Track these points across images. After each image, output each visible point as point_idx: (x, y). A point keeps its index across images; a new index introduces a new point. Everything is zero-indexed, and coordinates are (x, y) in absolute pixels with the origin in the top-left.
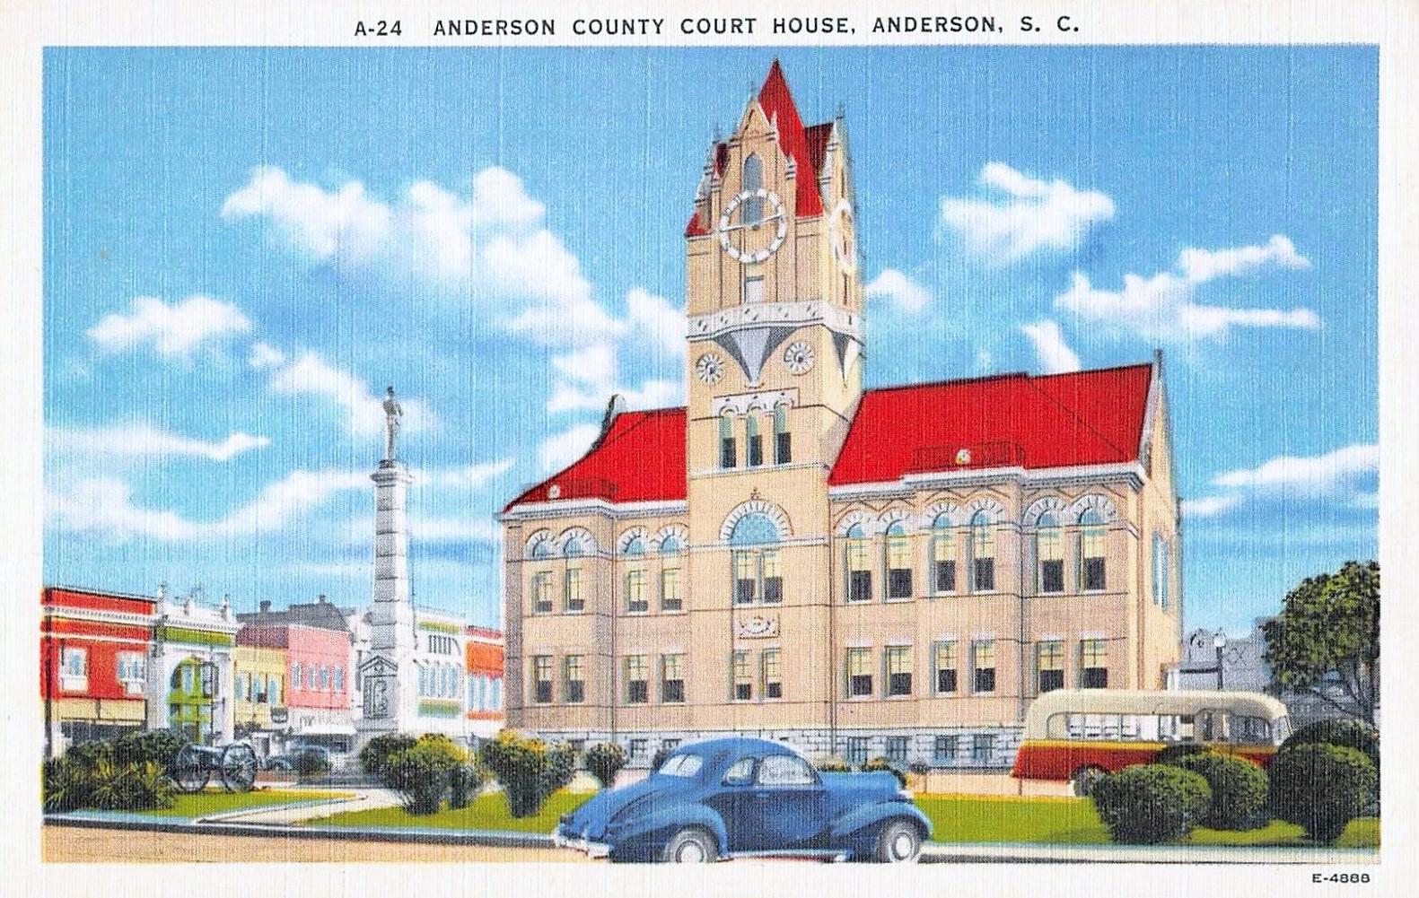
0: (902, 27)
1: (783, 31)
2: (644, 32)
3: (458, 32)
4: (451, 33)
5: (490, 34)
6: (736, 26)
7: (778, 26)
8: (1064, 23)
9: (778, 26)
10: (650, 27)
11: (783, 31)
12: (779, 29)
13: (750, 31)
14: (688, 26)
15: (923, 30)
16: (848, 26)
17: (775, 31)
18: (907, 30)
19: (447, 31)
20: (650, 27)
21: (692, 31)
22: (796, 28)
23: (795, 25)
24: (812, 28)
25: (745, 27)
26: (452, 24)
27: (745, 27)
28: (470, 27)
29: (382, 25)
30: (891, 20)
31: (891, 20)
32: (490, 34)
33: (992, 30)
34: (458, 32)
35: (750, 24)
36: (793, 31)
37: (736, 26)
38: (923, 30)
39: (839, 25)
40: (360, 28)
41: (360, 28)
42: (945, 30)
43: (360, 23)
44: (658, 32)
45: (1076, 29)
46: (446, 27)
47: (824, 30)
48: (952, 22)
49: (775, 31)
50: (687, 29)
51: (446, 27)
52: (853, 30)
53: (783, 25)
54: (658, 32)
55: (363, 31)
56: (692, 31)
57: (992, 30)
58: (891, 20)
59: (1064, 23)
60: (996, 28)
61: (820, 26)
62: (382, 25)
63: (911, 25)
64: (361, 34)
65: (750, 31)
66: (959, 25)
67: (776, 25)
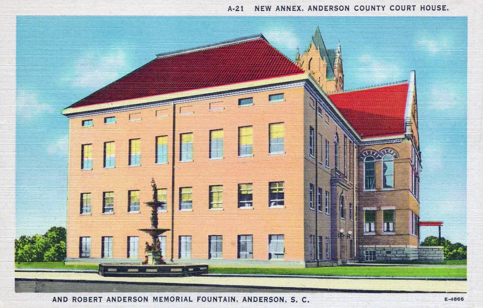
0: (63, 300)
1: (424, 10)
2: (378, 10)
3: (251, 301)
4: (248, 301)
5: (264, 11)
6: (409, 8)
7: (422, 8)
8: (304, 300)
9: (422, 8)
10: (381, 8)
11: (424, 10)
12: (423, 9)
13: (414, 10)
14: (392, 8)
15: (260, 301)
16: (446, 8)
17: (421, 10)
18: (320, 10)
19: (280, 10)
20: (381, 8)
21: (358, 10)
22: (321, 9)
23: (428, 8)
24: (210, 300)
25: (412, 8)
26: (314, 7)
27: (412, 8)
28: (321, 8)
29: (237, 7)
30: (282, 7)
31: (282, 7)
32: (264, 11)
33: (283, 301)
34: (251, 301)
35: (378, 8)
36: (429, 6)
37: (409, 8)
38: (260, 301)
39: (443, 8)
40: (230, 9)
41: (230, 9)
42: (267, 301)
43: (230, 7)
44: (383, 10)
45: (308, 302)
46: (312, 8)
47: (136, 297)
48: (440, 9)
49: (421, 10)
50: (304, 301)
51: (312, 8)
52: (448, 9)
53: (424, 8)
54: (383, 10)
55: (231, 9)
56: (358, 10)
57: (283, 301)
58: (282, 7)
59: (304, 300)
60: (284, 300)
61: (437, 8)
62: (237, 7)
63: (256, 300)
64: (230, 10)
65: (414, 10)
66: (272, 300)
67: (422, 8)
